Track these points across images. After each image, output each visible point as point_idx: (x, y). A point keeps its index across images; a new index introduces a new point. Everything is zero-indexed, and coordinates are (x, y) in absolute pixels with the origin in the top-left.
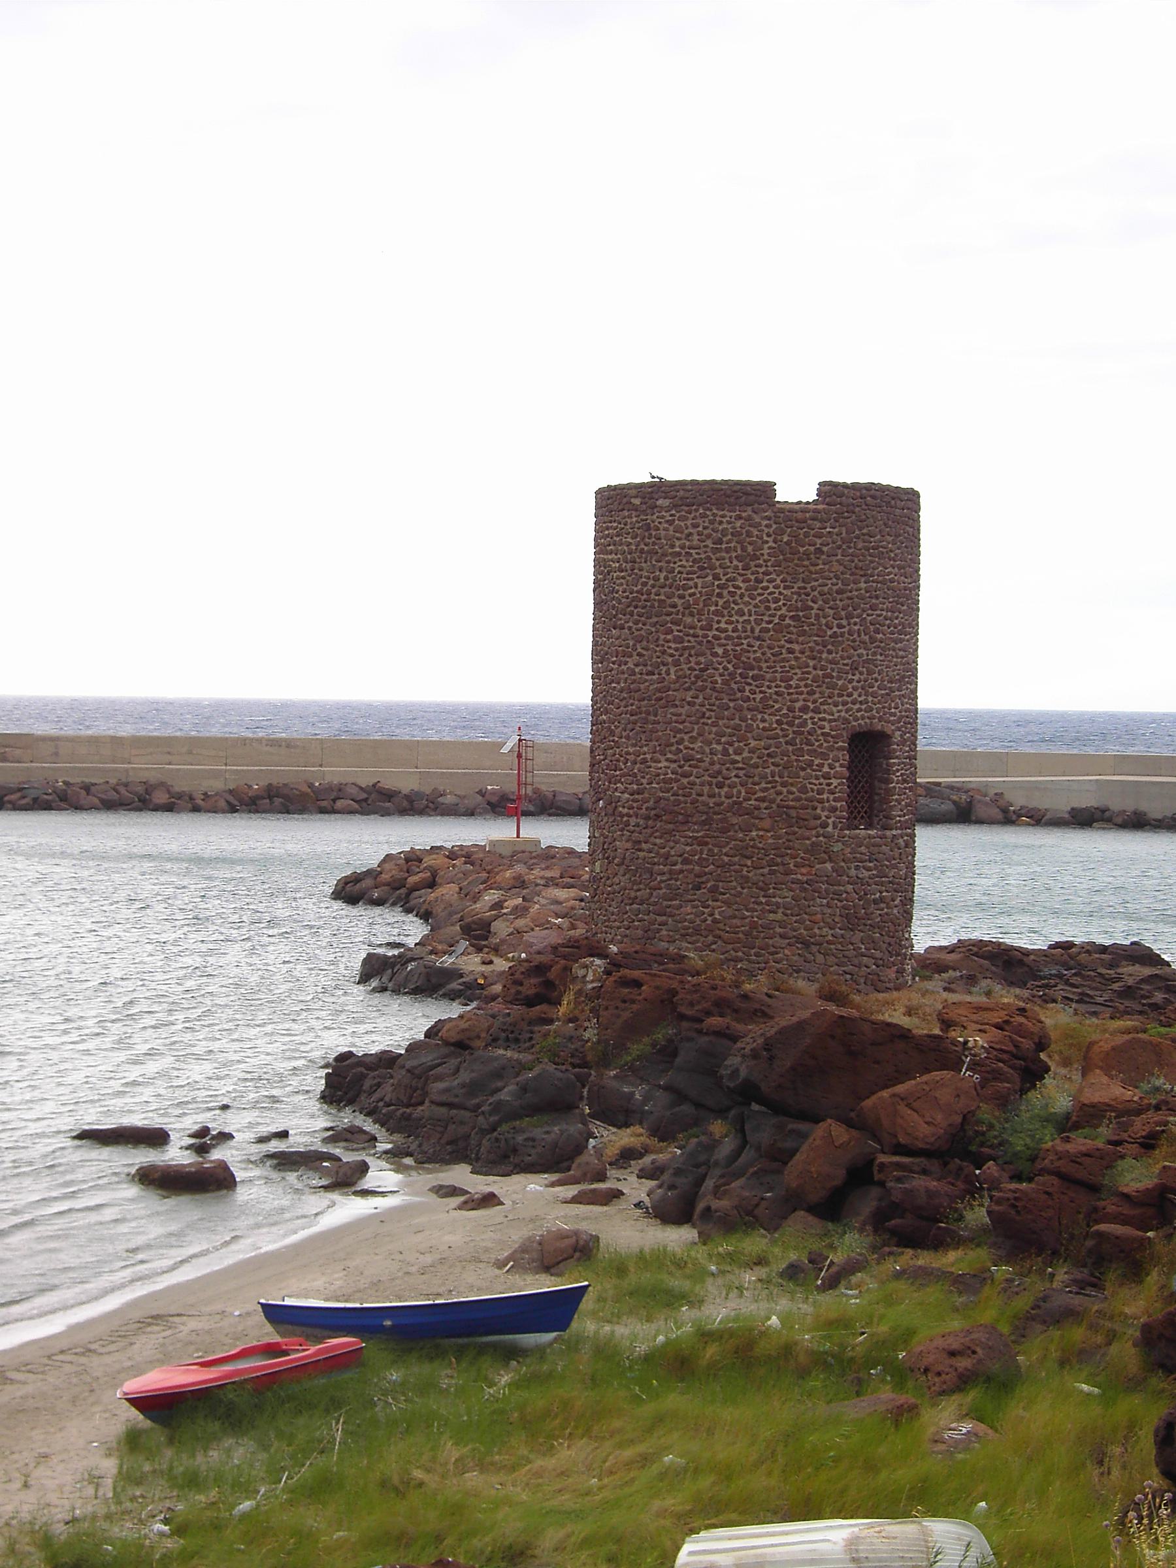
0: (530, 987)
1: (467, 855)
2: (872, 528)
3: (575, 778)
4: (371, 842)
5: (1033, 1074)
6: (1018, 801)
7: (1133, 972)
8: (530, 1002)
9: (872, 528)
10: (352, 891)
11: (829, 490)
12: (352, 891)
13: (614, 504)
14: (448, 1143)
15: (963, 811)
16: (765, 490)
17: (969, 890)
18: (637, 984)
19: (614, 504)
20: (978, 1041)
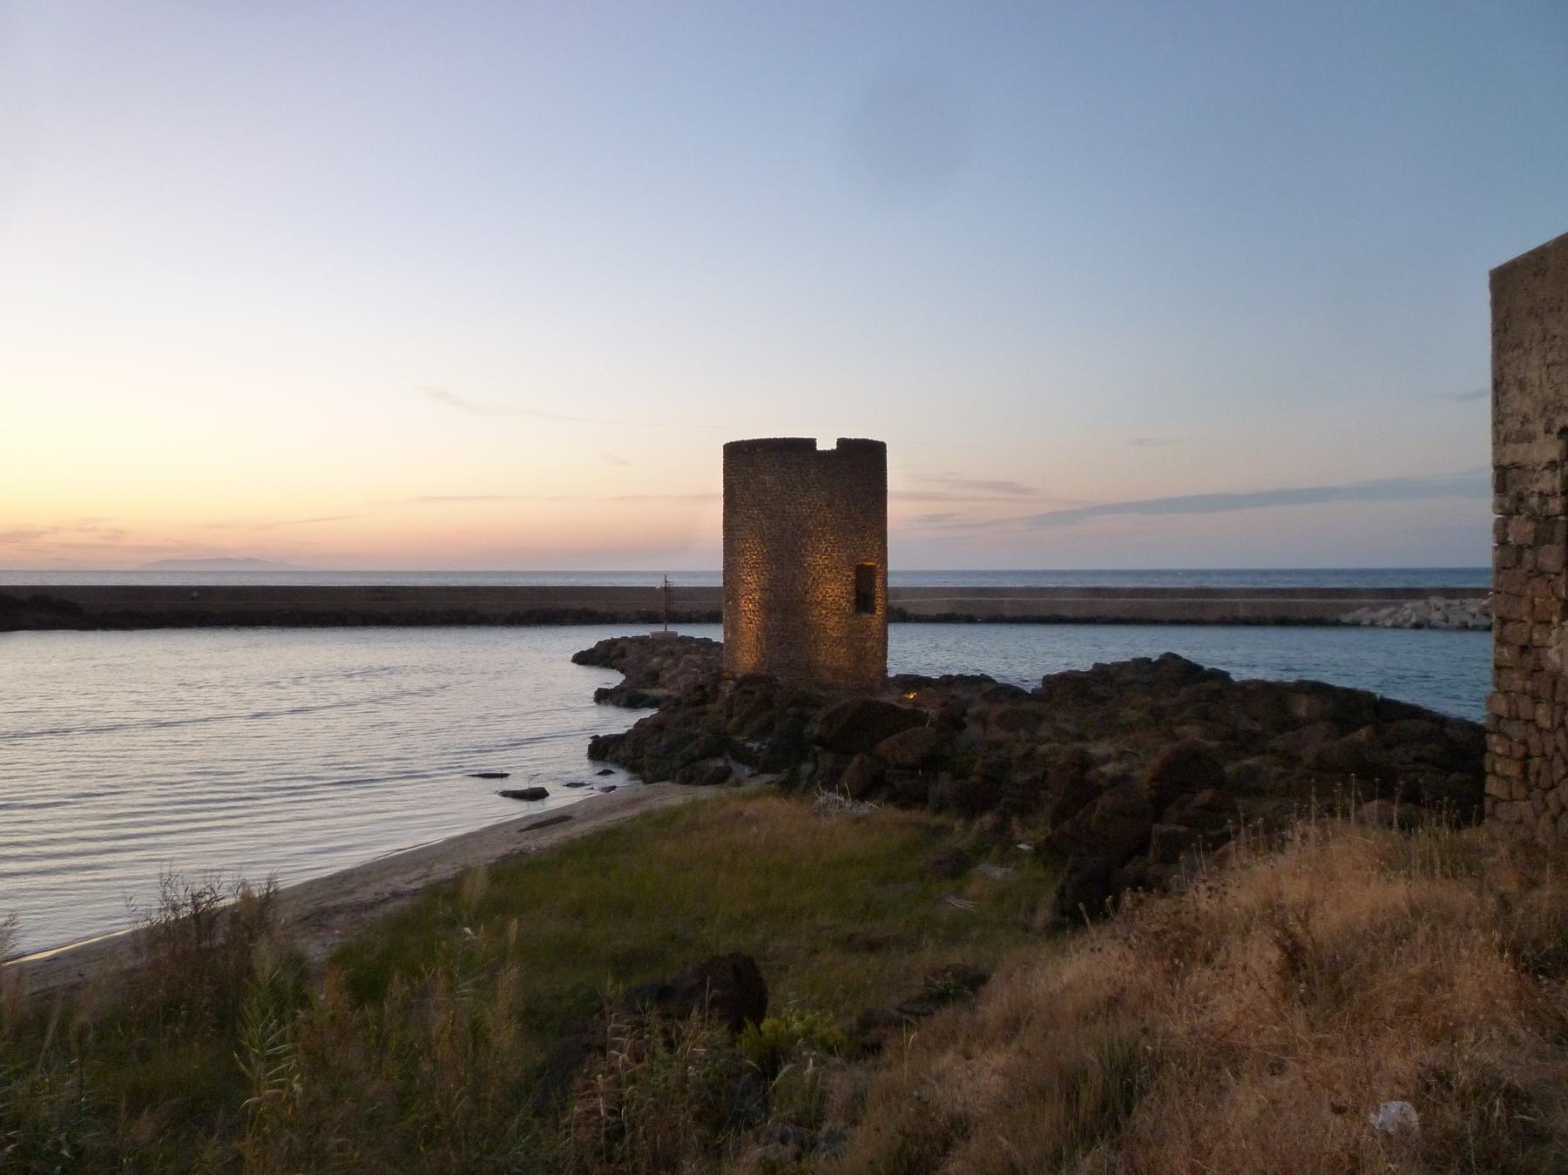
0: (697, 696)
1: (641, 641)
2: (863, 461)
3: (1486, 582)
4: (589, 638)
5: (960, 726)
6: (911, 611)
7: (987, 687)
8: (696, 704)
9: (863, 461)
10: (582, 659)
11: (842, 443)
12: (582, 659)
13: (738, 455)
14: (1102, 700)
15: (902, 617)
16: (811, 443)
17: (915, 652)
18: (752, 693)
19: (738, 455)
20: (932, 712)
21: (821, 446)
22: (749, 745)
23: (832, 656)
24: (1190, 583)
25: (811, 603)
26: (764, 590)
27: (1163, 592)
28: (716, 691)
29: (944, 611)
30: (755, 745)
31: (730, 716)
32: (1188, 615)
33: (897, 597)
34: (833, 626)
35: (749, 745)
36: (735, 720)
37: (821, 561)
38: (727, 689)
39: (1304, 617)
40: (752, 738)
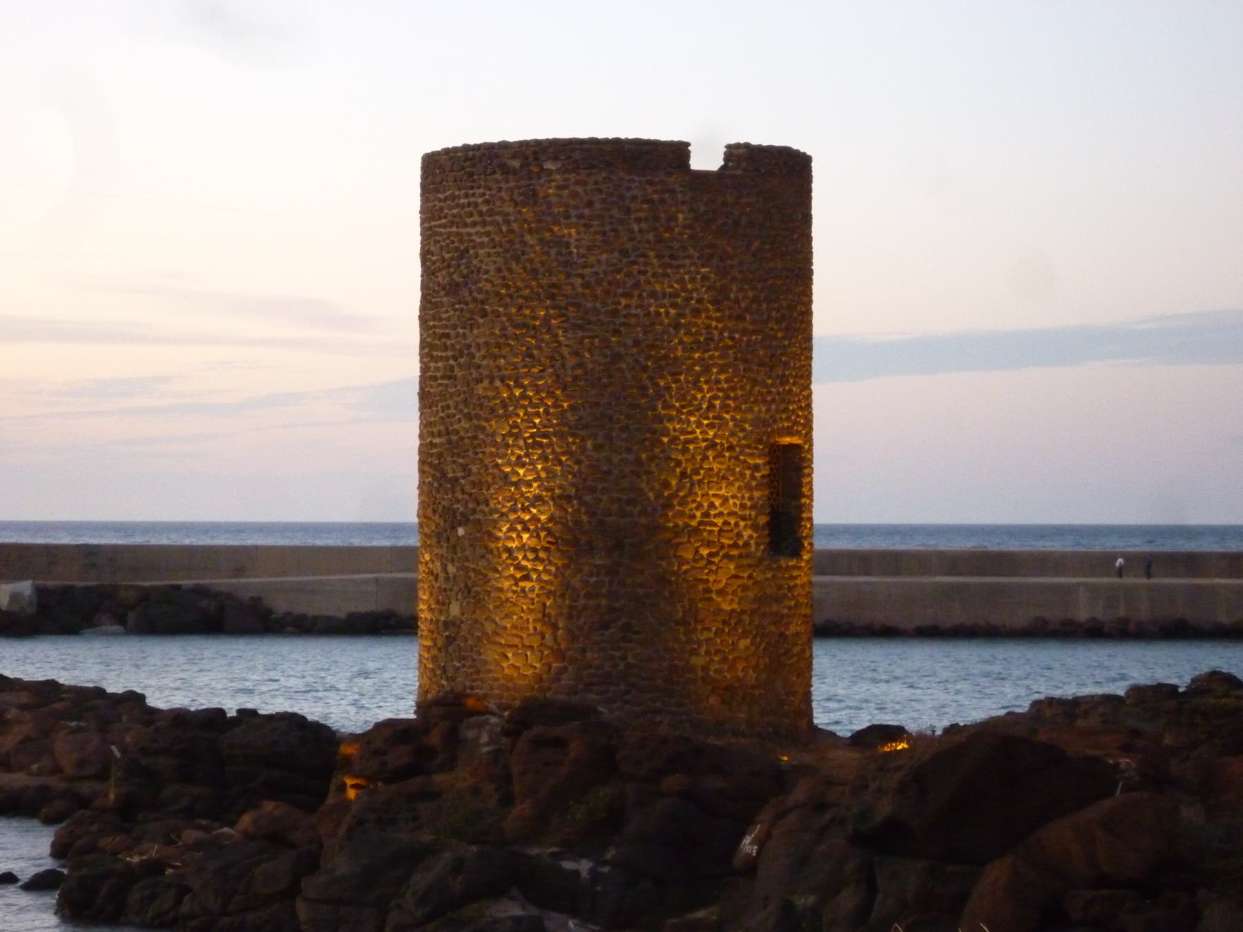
6: (281, 606)
9: (773, 183)
18: (560, 743)
21: (698, 163)
22: (568, 865)
23: (722, 655)
24: (968, 545)
25: (677, 531)
26: (562, 500)
27: (892, 562)
28: (453, 739)
29: (364, 607)
30: (584, 867)
31: (507, 800)
32: (959, 616)
33: (239, 571)
34: (723, 582)
35: (568, 865)
36: (522, 808)
37: (699, 430)
38: (482, 738)
39: (1224, 619)
40: (571, 848)
